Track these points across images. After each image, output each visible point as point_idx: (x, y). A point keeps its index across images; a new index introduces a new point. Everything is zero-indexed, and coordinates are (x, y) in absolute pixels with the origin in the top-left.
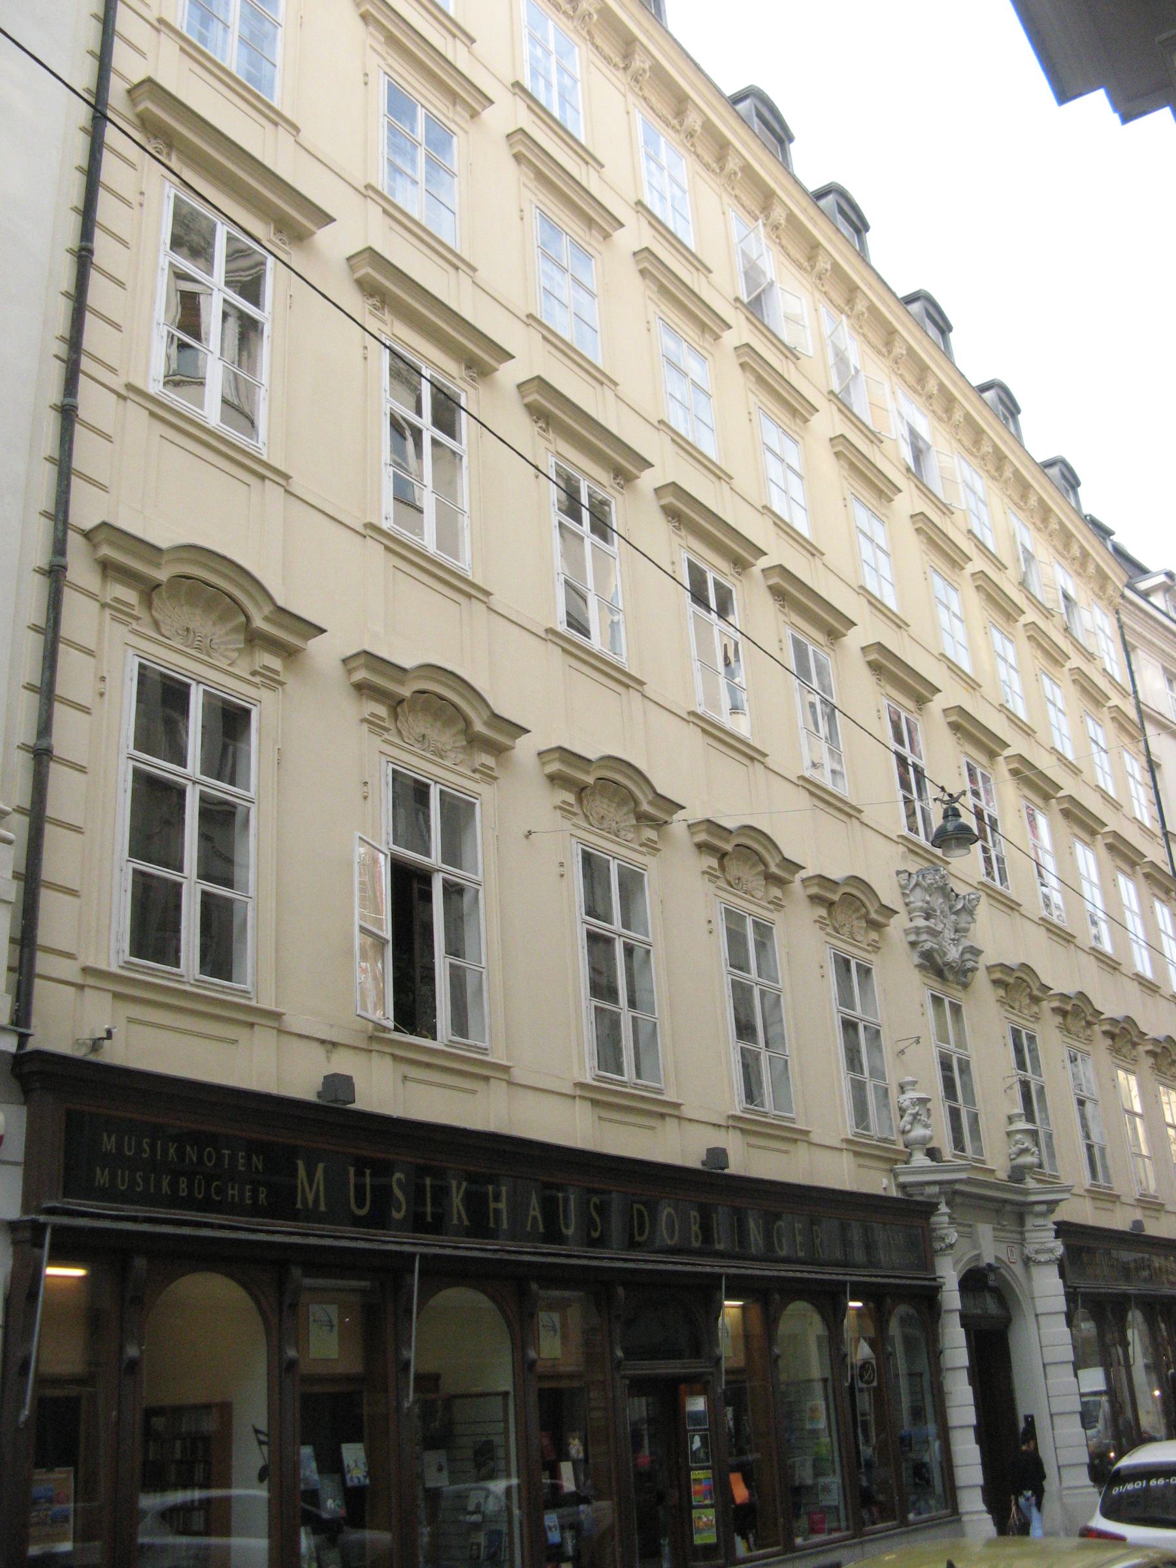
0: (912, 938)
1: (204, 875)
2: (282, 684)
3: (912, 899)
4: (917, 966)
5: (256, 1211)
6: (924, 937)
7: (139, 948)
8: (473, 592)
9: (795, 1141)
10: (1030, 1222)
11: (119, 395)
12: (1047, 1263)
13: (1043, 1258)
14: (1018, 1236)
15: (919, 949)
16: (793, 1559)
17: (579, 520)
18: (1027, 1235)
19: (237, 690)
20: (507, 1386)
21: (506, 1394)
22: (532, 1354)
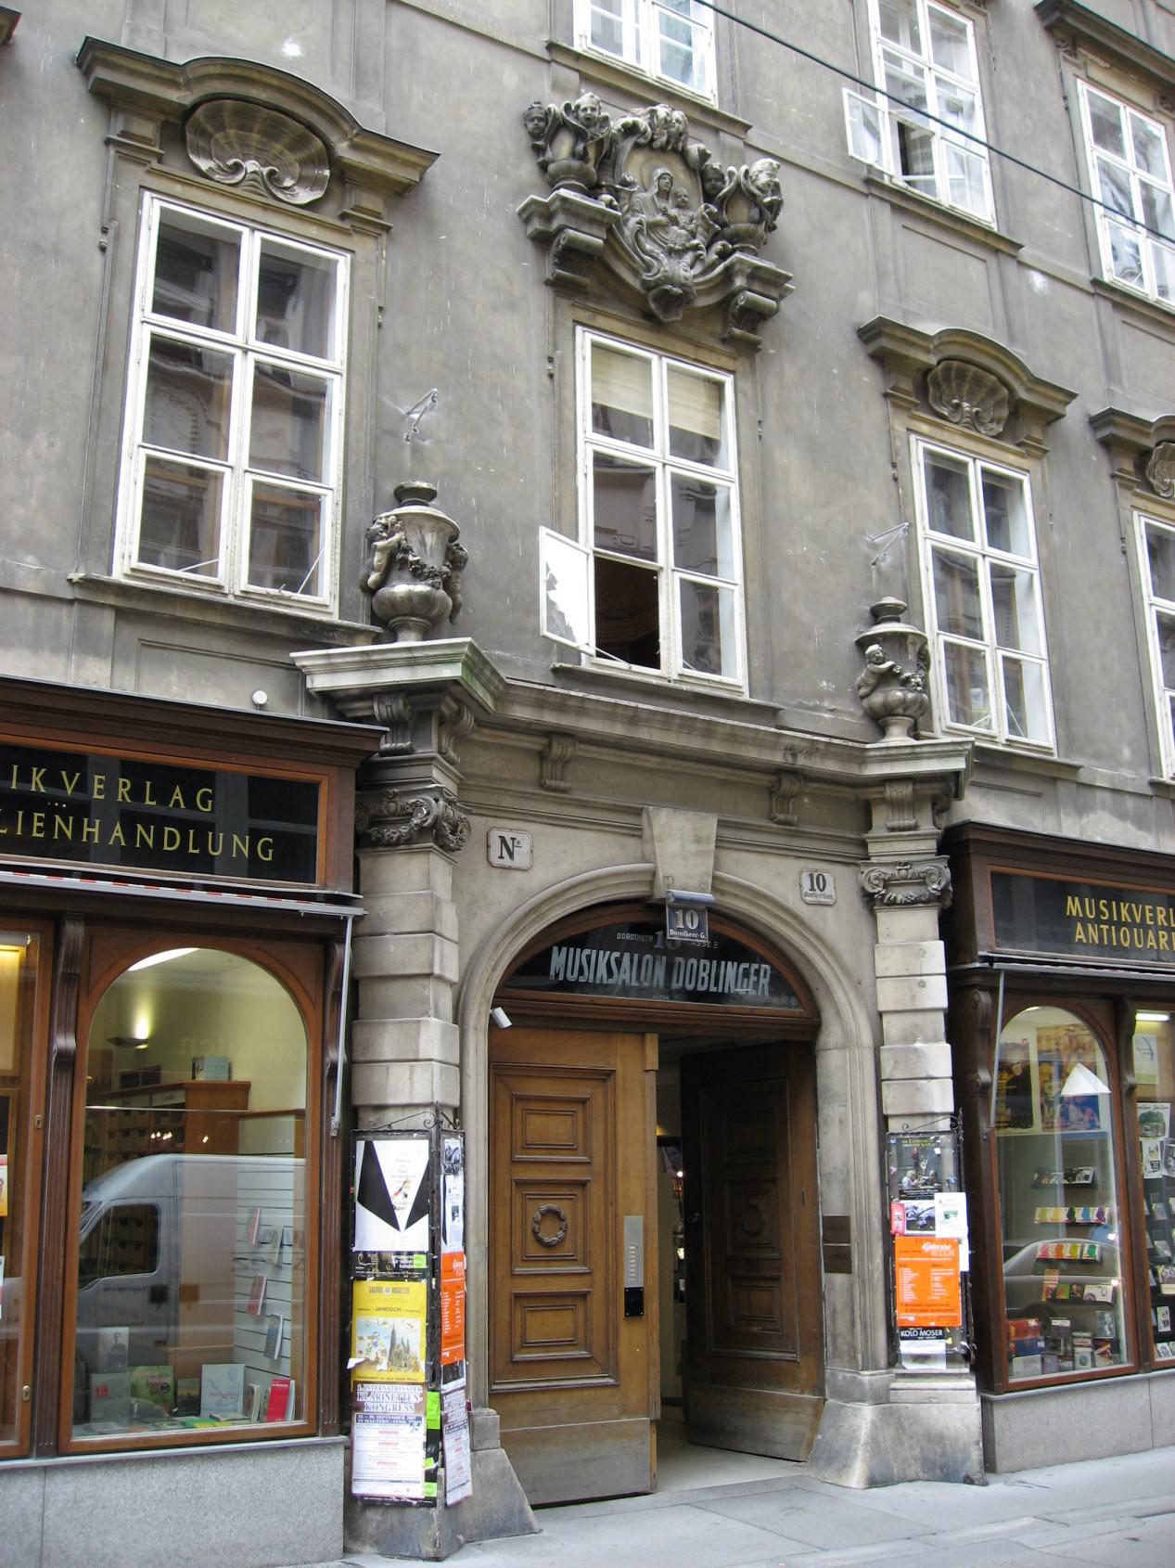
0: (537, 225)
1: (949, 625)
2: (388, 229)
3: (549, 154)
4: (548, 283)
5: (255, 868)
6: (559, 221)
7: (609, 641)
8: (1002, 247)
9: (1054, 780)
10: (881, 819)
11: (1088, 293)
12: (911, 904)
13: (899, 894)
14: (852, 850)
15: (554, 249)
16: (1149, 1380)
17: (1118, 149)
18: (873, 849)
19: (300, 243)
20: (300, 1102)
21: (299, 1114)
22: (1130, 1080)
